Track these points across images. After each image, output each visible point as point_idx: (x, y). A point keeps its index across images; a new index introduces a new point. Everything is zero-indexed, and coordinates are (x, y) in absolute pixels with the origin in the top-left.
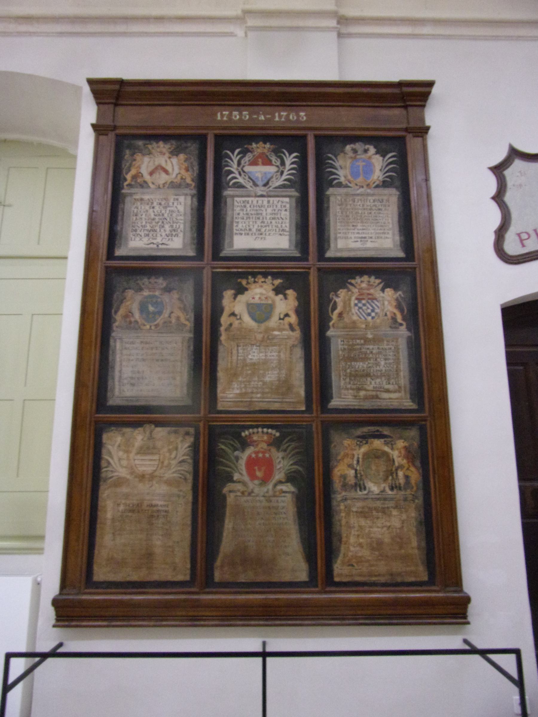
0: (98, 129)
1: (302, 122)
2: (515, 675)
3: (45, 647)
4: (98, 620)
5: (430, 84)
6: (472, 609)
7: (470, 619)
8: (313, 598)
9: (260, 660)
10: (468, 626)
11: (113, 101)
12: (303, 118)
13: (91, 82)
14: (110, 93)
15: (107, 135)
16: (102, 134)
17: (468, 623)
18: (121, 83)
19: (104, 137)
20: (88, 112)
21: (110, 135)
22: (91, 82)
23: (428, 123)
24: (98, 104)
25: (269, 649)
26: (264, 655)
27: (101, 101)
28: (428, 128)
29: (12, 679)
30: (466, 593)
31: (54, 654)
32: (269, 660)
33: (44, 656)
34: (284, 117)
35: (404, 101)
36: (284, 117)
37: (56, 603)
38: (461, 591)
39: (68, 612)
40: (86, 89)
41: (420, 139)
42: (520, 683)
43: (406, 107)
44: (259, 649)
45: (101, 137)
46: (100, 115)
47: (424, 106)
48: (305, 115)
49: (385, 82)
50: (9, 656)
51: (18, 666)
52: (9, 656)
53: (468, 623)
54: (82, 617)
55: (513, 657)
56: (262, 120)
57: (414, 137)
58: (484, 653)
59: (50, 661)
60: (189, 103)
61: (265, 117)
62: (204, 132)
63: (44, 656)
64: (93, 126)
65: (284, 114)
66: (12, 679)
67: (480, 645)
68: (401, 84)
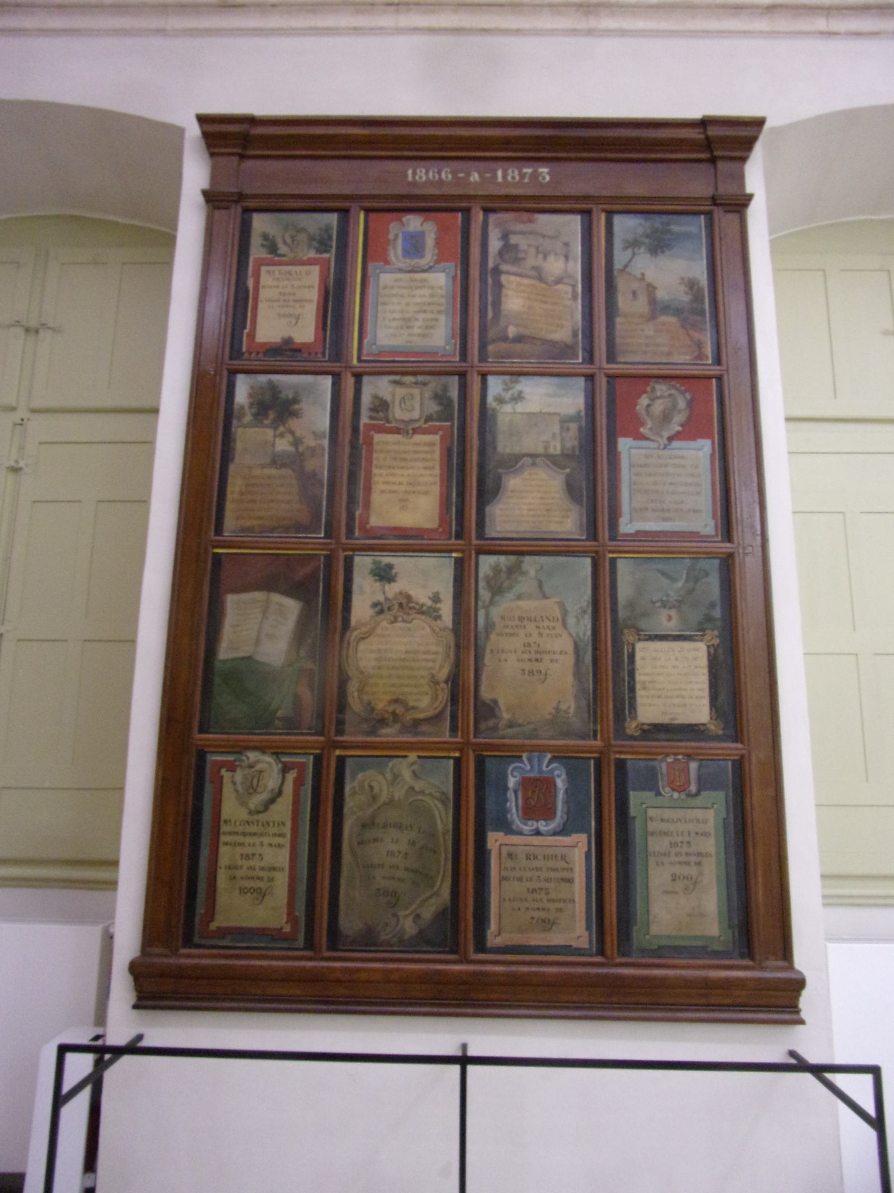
0: (212, 198)
1: (542, 186)
2: (871, 1110)
3: (117, 1036)
4: (687, 1010)
5: (758, 123)
6: (805, 1001)
7: (804, 1015)
8: (270, 966)
9: (456, 1069)
10: (800, 1027)
11: (239, 151)
12: (544, 178)
13: (203, 120)
14: (227, 136)
15: (227, 208)
16: (219, 208)
17: (802, 1022)
18: (251, 120)
19: (224, 212)
20: (195, 174)
21: (233, 210)
22: (203, 120)
23: (749, 190)
24: (212, 155)
25: (472, 1052)
26: (464, 1061)
27: (217, 150)
28: (750, 197)
29: (68, 1085)
30: (800, 973)
31: (134, 1048)
32: (471, 1069)
33: (118, 1052)
34: (528, 176)
35: (245, 147)
36: (528, 176)
37: (134, 968)
38: (791, 967)
39: (161, 985)
40: (194, 131)
41: (733, 217)
42: (878, 1123)
43: (713, 161)
44: (456, 1052)
45: (217, 213)
46: (214, 177)
47: (744, 159)
48: (549, 173)
49: (735, 117)
50: (63, 1050)
51: (79, 1066)
52: (875, 1071)
53: (802, 1022)
54: (759, 1006)
55: (868, 1078)
56: (476, 182)
57: (726, 212)
58: (819, 1071)
59: (126, 1060)
60: (487, 154)
61: (481, 177)
62: (346, 204)
63: (118, 1052)
64: (205, 193)
65: (528, 170)
66: (68, 1085)
67: (813, 1058)
68: (704, 123)
